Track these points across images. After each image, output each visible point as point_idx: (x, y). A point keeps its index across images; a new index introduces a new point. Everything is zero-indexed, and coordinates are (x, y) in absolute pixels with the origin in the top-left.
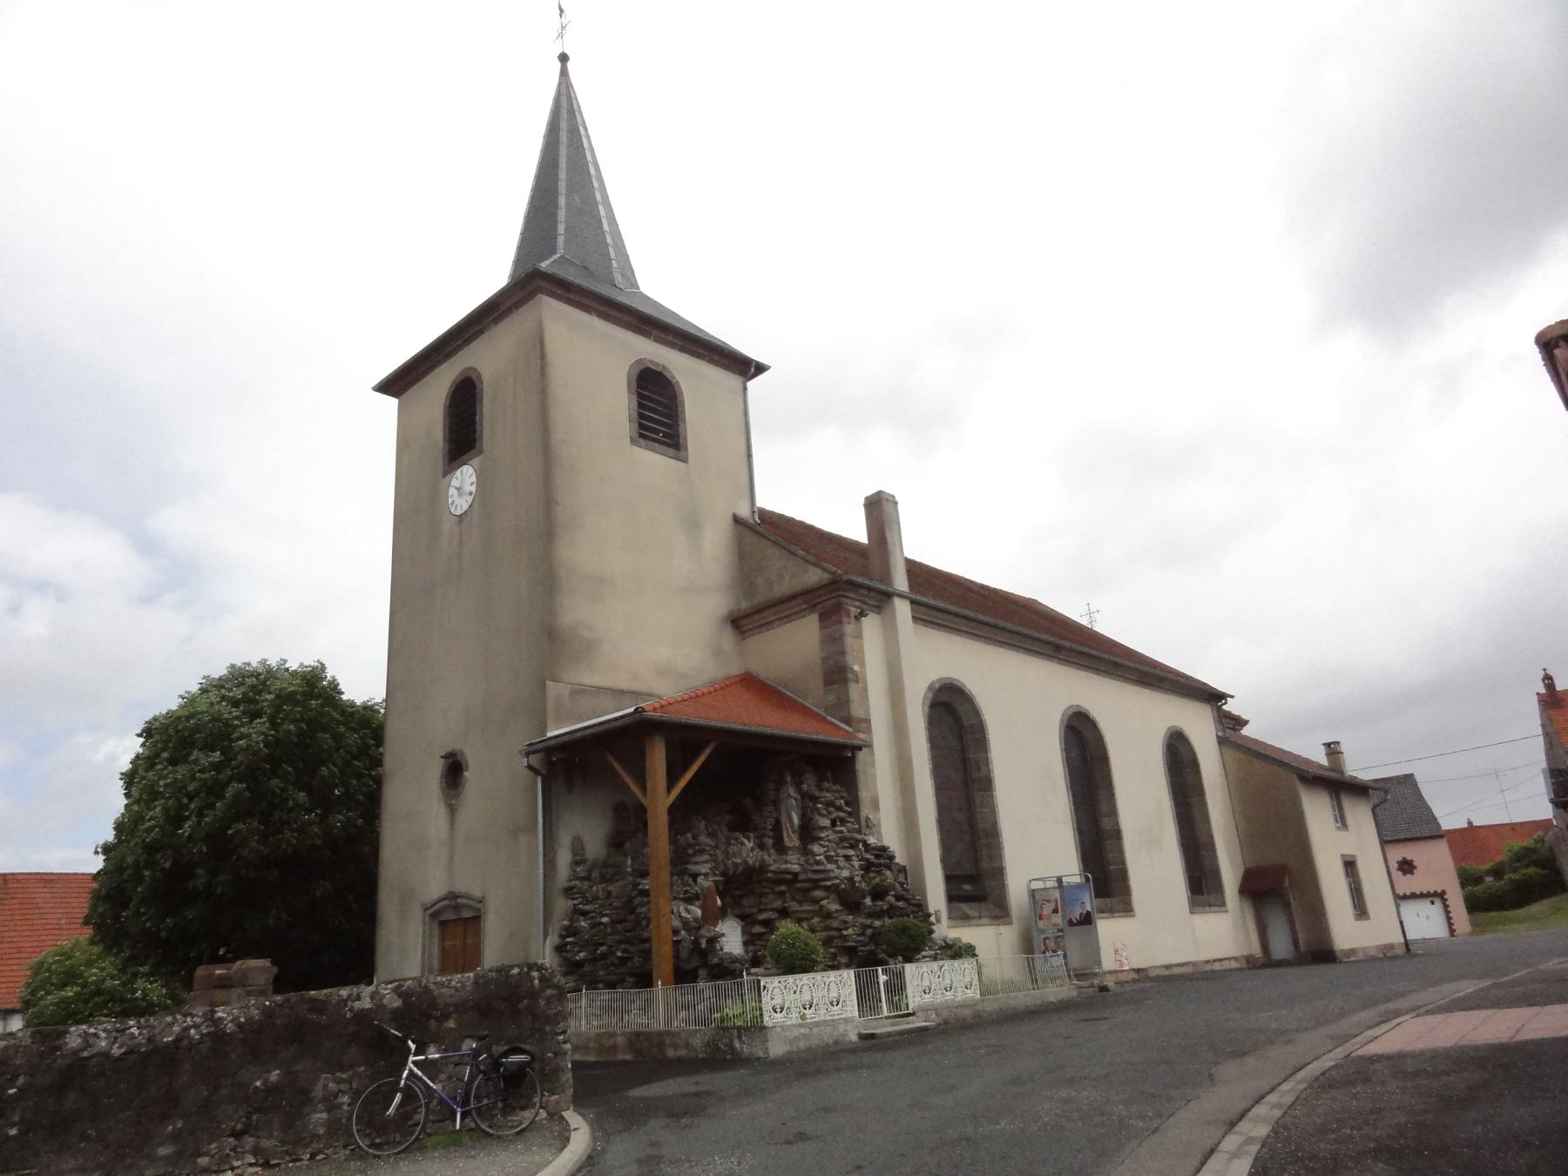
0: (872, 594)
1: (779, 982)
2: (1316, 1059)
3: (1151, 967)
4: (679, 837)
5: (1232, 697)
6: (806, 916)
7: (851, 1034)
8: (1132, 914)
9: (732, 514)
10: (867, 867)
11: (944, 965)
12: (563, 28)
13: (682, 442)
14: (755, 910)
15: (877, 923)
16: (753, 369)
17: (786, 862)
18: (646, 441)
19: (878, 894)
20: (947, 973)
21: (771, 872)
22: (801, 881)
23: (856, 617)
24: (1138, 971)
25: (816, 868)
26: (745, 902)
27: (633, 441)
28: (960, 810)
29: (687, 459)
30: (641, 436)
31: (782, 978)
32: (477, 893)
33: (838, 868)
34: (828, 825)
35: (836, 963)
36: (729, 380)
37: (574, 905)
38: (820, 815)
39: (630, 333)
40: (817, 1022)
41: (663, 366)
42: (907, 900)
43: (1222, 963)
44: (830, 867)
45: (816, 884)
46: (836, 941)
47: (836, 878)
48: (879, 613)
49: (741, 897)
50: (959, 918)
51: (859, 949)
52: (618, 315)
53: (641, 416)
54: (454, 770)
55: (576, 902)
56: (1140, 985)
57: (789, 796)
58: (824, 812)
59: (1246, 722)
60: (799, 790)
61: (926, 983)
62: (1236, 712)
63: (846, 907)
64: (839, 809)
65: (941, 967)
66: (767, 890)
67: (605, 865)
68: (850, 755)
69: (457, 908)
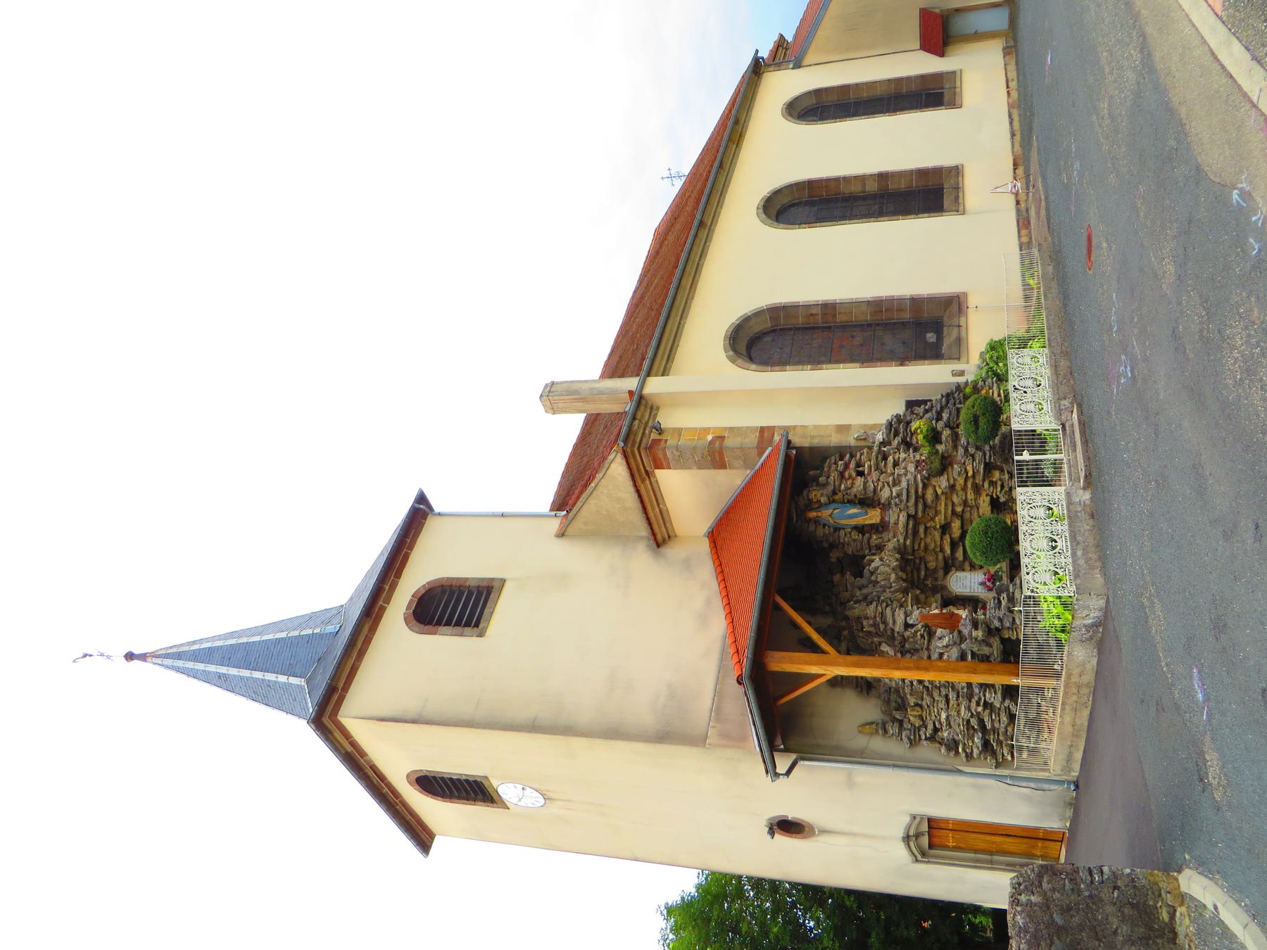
0: (639, 416)
1: (1028, 574)
2: (1216, 58)
3: (1013, 152)
4: (865, 630)
5: (757, 51)
6: (950, 509)
7: (1084, 498)
8: (960, 167)
9: (556, 538)
10: (907, 444)
11: (1014, 386)
12: (102, 655)
13: (485, 584)
14: (940, 556)
15: (963, 441)
16: (421, 506)
17: (896, 524)
18: (482, 621)
19: (934, 437)
20: (1022, 383)
21: (905, 540)
22: (916, 512)
23: (660, 434)
24: (1016, 165)
25: (904, 497)
26: (932, 565)
27: (481, 635)
28: (853, 337)
29: (502, 579)
30: (477, 625)
31: (1024, 570)
32: (907, 819)
33: (906, 475)
34: (863, 480)
35: (999, 483)
36: (431, 525)
37: (926, 739)
38: (852, 487)
39: (366, 656)
40: (1070, 535)
41: (412, 596)
42: (942, 409)
43: (1010, 78)
44: (904, 484)
45: (920, 498)
46: (977, 481)
47: (915, 478)
48: (658, 408)
49: (927, 568)
50: (958, 350)
51: (987, 460)
52: (362, 638)
53: (458, 624)
54: (787, 826)
55: (923, 737)
56: (1034, 167)
57: (830, 515)
58: (849, 482)
59: (781, 36)
60: (827, 505)
61: (1031, 407)
62: (770, 46)
63: (945, 470)
64: (847, 466)
65: (1016, 389)
66: (923, 544)
67: (888, 702)
68: (794, 452)
69: (918, 836)
